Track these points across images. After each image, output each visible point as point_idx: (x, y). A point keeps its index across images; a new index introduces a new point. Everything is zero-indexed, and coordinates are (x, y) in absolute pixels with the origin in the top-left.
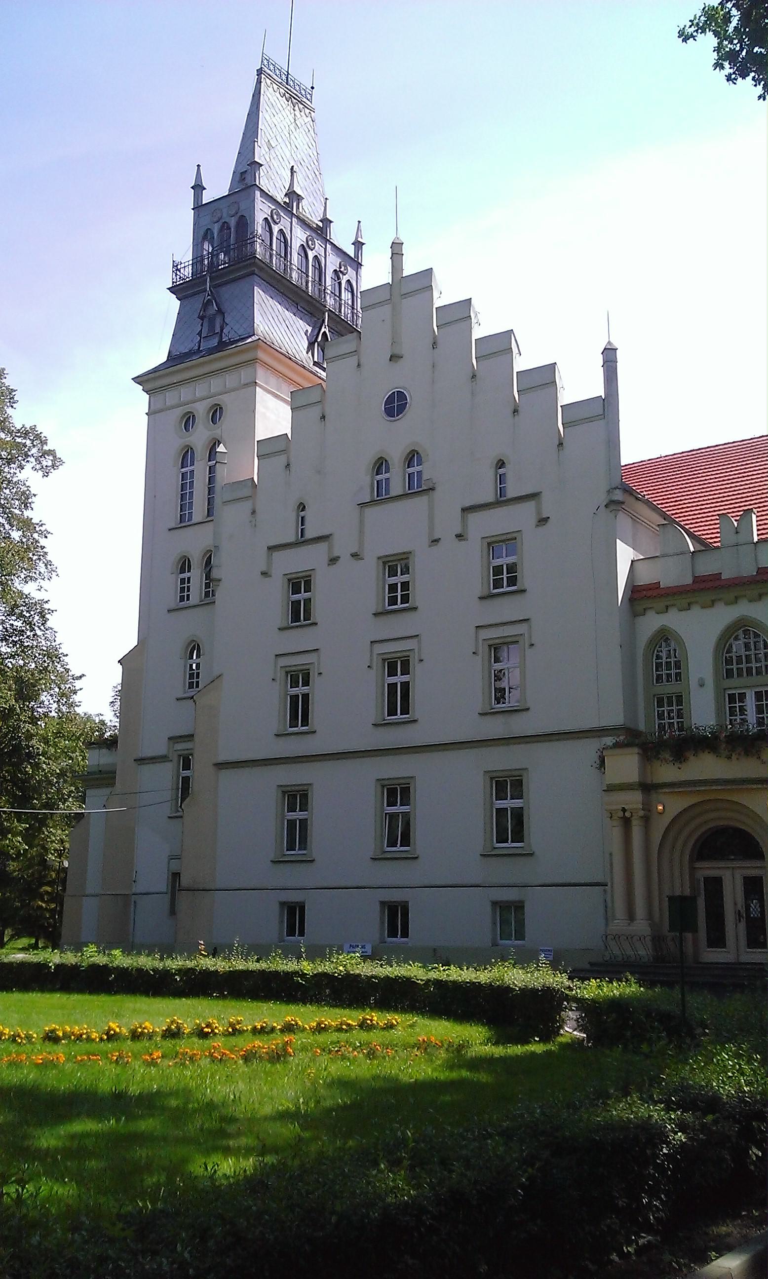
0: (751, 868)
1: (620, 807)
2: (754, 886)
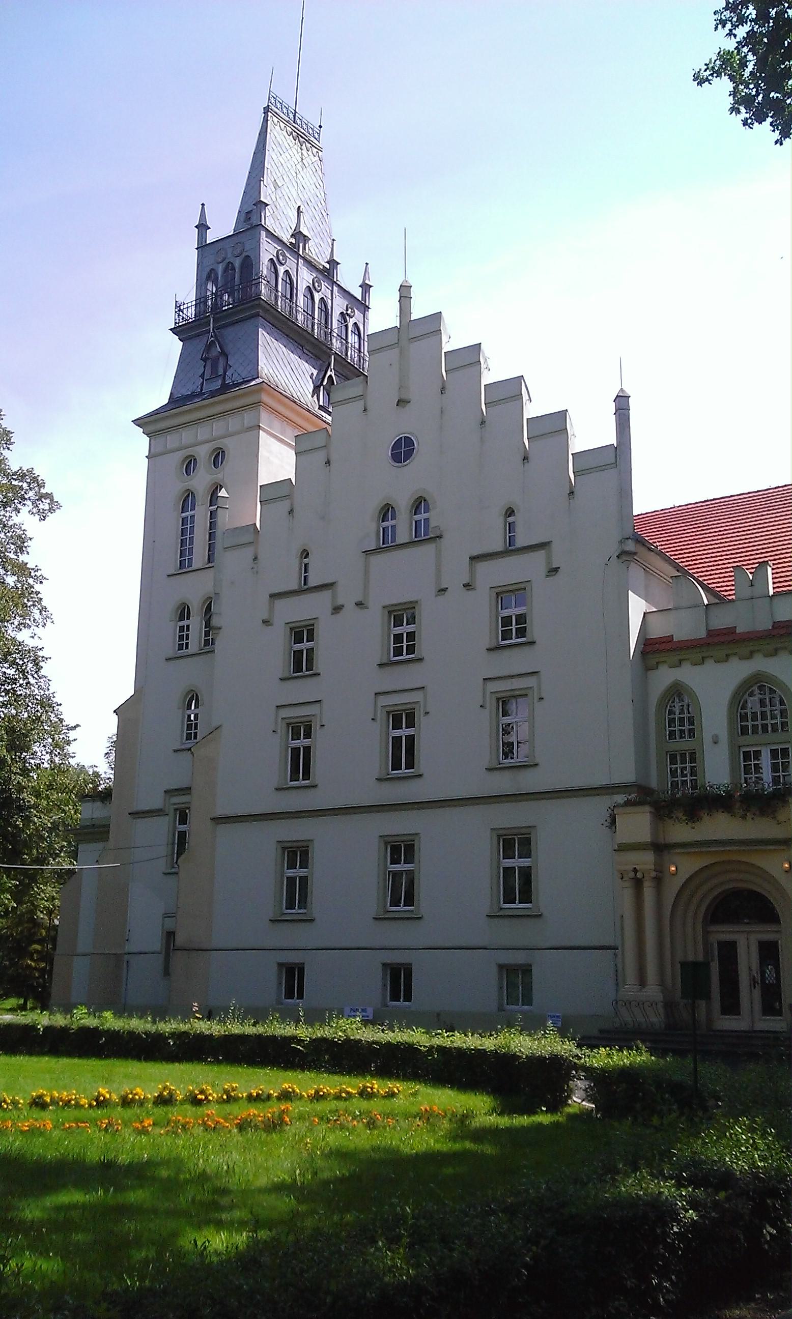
0: (765, 933)
1: (631, 867)
2: (769, 952)
